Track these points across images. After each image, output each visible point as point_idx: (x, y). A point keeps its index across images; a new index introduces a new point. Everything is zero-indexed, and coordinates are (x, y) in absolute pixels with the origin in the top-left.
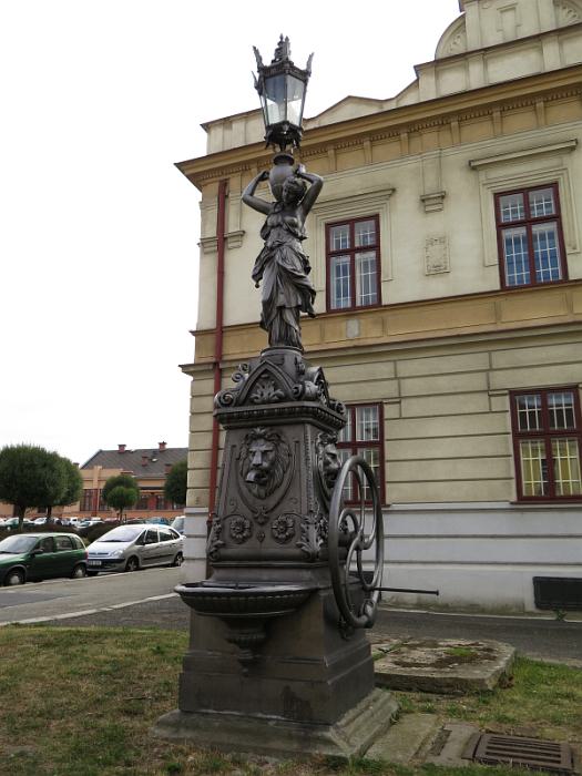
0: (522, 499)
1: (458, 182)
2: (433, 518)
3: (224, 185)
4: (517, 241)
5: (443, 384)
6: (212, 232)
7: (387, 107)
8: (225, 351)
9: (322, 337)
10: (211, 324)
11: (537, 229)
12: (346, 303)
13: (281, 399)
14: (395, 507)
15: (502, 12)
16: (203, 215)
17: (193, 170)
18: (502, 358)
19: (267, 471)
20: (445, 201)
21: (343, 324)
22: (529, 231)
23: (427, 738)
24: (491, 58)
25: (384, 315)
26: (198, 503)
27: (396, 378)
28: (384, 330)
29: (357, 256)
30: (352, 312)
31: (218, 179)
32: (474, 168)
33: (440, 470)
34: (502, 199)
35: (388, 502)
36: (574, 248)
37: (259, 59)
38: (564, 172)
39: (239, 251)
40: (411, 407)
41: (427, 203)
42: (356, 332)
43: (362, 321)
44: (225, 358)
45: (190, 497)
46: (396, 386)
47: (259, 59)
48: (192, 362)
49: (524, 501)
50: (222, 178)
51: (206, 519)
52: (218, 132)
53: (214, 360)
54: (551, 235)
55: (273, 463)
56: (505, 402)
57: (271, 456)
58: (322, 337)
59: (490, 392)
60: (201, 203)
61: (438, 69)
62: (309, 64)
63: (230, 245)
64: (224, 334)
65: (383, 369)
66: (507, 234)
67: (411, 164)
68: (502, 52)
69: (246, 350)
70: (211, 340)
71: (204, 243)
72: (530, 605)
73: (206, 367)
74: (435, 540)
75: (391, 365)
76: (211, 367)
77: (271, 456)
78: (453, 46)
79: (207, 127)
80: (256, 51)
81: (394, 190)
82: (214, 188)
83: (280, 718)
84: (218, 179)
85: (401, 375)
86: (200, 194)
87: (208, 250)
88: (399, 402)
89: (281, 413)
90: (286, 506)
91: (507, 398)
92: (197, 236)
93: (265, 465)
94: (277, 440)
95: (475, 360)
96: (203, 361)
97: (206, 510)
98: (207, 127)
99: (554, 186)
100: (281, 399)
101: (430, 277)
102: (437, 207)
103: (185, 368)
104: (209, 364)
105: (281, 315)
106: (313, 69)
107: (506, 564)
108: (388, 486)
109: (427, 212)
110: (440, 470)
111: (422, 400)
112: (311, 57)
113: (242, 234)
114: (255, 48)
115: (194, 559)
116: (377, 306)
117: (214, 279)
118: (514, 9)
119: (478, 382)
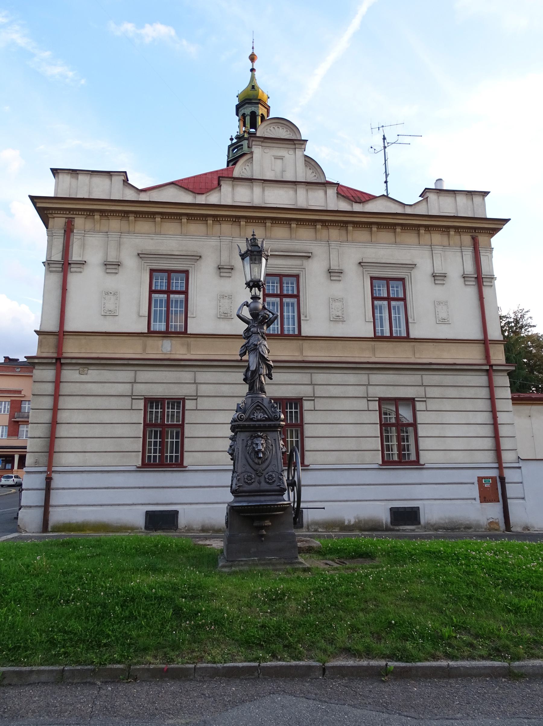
0: (384, 462)
2: (214, 475)
4: (161, 301)
7: (409, 211)
8: (64, 350)
9: (144, 349)
11: (285, 300)
12: (160, 326)
14: (190, 468)
15: (275, 158)
17: (45, 208)
18: (145, 375)
20: (233, 271)
21: (160, 342)
22: (168, 297)
24: (267, 186)
25: (189, 340)
26: (36, 463)
27: (195, 383)
28: (189, 350)
29: (172, 296)
30: (167, 334)
34: (155, 274)
35: (185, 464)
36: (306, 317)
38: (304, 270)
39: (79, 275)
41: (222, 270)
42: (169, 349)
43: (174, 342)
44: (65, 355)
46: (195, 388)
49: (387, 463)
51: (44, 476)
52: (66, 179)
54: (293, 305)
56: (375, 405)
58: (144, 349)
59: (133, 397)
61: (235, 183)
63: (72, 270)
65: (186, 375)
66: (155, 296)
67: (213, 242)
68: (273, 185)
69: (83, 351)
70: (52, 340)
71: (48, 264)
73: (50, 361)
74: (215, 489)
75: (132, 374)
76: (54, 361)
78: (244, 170)
79: (55, 172)
81: (200, 257)
85: (310, 386)
87: (51, 269)
88: (197, 399)
90: (270, 468)
91: (377, 403)
95: (126, 375)
96: (44, 355)
98: (55, 172)
99: (297, 276)
102: (114, 271)
104: (52, 358)
107: (89, 505)
108: (186, 454)
109: (221, 276)
111: (211, 399)
113: (83, 263)
115: (30, 507)
116: (184, 333)
117: (58, 293)
118: (282, 159)
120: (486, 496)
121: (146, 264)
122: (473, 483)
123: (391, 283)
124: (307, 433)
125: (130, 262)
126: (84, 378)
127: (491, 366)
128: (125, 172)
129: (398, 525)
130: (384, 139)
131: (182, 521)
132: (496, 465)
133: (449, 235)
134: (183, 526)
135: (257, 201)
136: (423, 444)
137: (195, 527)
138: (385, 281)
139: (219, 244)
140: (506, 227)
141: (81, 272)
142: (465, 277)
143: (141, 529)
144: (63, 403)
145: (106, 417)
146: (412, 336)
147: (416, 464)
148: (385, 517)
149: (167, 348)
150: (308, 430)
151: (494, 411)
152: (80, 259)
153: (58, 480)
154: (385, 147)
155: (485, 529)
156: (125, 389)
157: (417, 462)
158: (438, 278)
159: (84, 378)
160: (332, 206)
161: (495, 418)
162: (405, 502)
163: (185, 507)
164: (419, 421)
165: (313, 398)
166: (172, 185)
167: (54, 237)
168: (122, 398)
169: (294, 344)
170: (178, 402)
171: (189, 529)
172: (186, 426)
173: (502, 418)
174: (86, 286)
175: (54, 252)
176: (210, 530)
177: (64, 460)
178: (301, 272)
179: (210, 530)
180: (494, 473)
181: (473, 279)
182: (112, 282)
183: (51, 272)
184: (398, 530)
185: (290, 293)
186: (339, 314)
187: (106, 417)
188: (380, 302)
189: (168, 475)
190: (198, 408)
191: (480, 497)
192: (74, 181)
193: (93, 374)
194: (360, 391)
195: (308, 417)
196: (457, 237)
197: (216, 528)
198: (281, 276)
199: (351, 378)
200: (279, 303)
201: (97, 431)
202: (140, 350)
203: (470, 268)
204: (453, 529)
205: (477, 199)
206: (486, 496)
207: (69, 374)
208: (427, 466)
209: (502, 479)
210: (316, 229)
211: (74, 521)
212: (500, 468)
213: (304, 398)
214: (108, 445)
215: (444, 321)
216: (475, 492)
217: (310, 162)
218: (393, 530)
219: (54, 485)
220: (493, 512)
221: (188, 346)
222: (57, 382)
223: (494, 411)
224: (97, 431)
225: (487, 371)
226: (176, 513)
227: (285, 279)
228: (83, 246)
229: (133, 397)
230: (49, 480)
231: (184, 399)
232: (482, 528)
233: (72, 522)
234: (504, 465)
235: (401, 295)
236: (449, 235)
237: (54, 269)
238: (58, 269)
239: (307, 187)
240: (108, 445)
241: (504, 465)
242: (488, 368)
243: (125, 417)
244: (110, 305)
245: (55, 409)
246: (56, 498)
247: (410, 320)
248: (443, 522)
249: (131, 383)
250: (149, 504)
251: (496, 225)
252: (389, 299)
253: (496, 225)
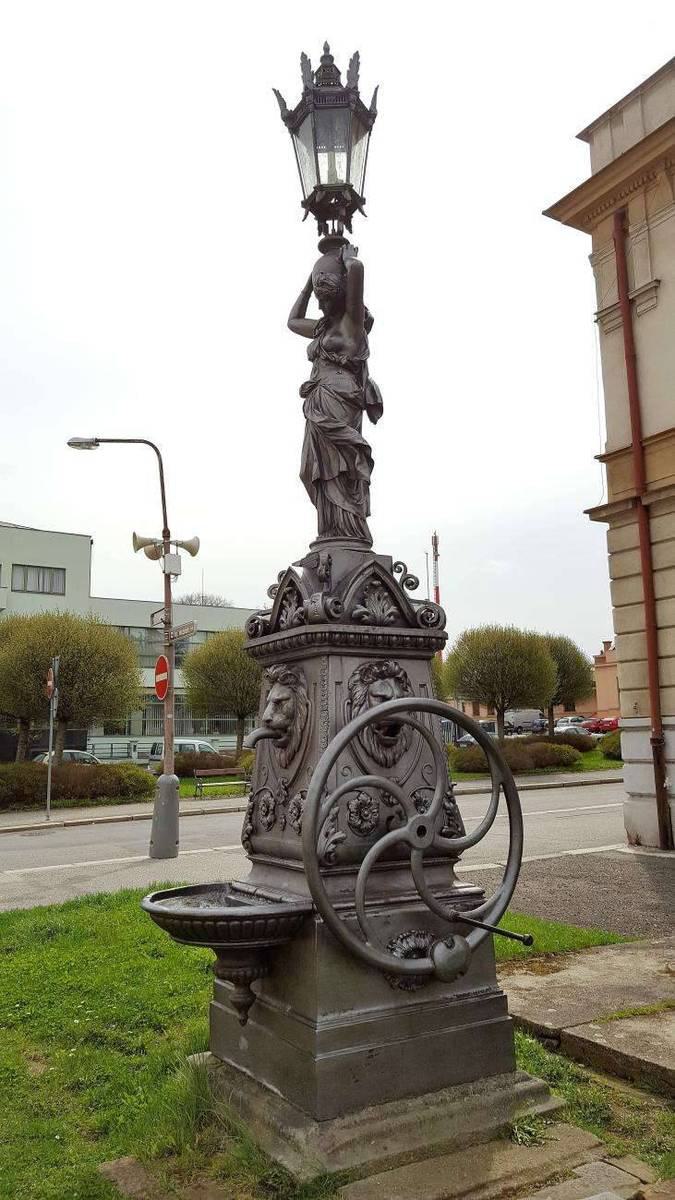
3: (622, 218)
6: (613, 297)
10: (626, 439)
16: (598, 275)
17: (569, 211)
19: (284, 729)
23: (348, 1127)
31: (611, 211)
37: (282, 103)
47: (282, 103)
48: (605, 501)
51: (649, 735)
52: (604, 135)
53: (634, 494)
55: (291, 716)
57: (288, 705)
60: (591, 257)
63: (639, 310)
64: (648, 451)
70: (628, 464)
71: (602, 317)
77: (288, 705)
79: (586, 135)
80: (277, 93)
82: (608, 227)
83: (279, 1093)
84: (611, 211)
86: (589, 237)
92: (592, 306)
93: (278, 719)
94: (290, 682)
96: (622, 497)
97: (648, 722)
98: (586, 135)
103: (595, 514)
104: (626, 501)
105: (322, 492)
106: (378, 107)
112: (377, 89)
114: (274, 90)
117: (623, 371)
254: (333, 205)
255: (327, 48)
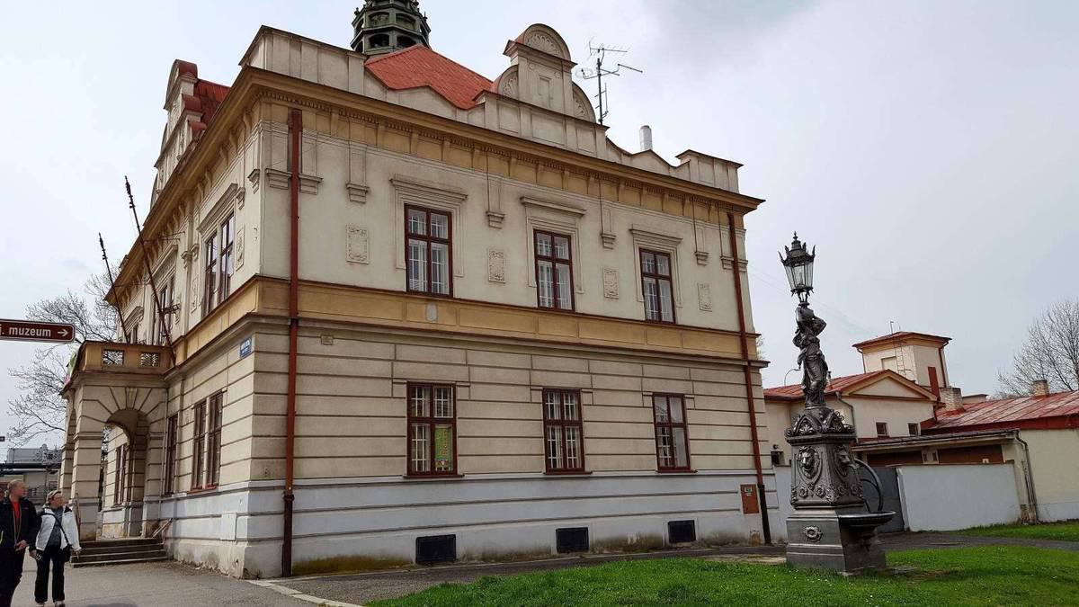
0: (661, 469)
1: (512, 210)
2: (492, 486)
5: (501, 375)
7: (626, 161)
9: (405, 315)
12: (420, 284)
13: (814, 433)
18: (407, 351)
27: (589, 373)
28: (458, 322)
29: (433, 244)
32: (524, 204)
33: (499, 446)
36: (580, 289)
40: (478, 391)
43: (440, 308)
45: (226, 477)
50: (295, 106)
58: (405, 315)
59: (393, 380)
62: (813, 252)
65: (456, 355)
67: (479, 178)
70: (281, 292)
71: (746, 263)
72: (554, 552)
75: (391, 349)
78: (507, 87)
89: (813, 440)
95: (382, 349)
99: (569, 237)
100: (814, 433)
101: (607, 299)
103: (766, 364)
110: (499, 446)
113: (317, 182)
117: (283, 221)
118: (548, 81)
119: (522, 377)
120: (748, 508)
121: (401, 196)
122: (737, 493)
123: (433, 215)
124: (587, 433)
125: (381, 190)
126: (328, 350)
127: (749, 362)
128: (266, 32)
129: (676, 543)
130: (599, 64)
131: (461, 548)
132: (755, 472)
133: (442, 145)
134: (461, 555)
135: (525, 133)
136: (695, 447)
137: (475, 555)
138: (425, 213)
139: (485, 182)
140: (760, 206)
141: (315, 194)
142: (723, 259)
143: (412, 562)
144: (304, 385)
145: (361, 407)
146: (456, 295)
147: (687, 471)
148: (664, 533)
149: (431, 315)
150: (589, 429)
151: (751, 412)
152: (313, 174)
153: (301, 500)
154: (600, 75)
155: (749, 543)
156: (383, 368)
157: (687, 469)
158: (701, 257)
159: (328, 350)
160: (356, 88)
161: (753, 419)
162: (678, 515)
163: (463, 529)
164: (689, 420)
165: (591, 390)
166: (426, 90)
167: (273, 134)
168: (381, 381)
169: (570, 322)
170: (446, 389)
171: (468, 557)
172: (458, 422)
173: (759, 419)
174: (325, 212)
175: (275, 156)
176: (491, 559)
177: (307, 469)
178: (454, 210)
179: (491, 559)
180: (753, 481)
181: (730, 263)
182: (357, 215)
183: (272, 186)
184: (676, 548)
185: (545, 254)
186: (613, 289)
187: (361, 407)
188: (416, 242)
189: (442, 487)
190: (472, 398)
191: (744, 507)
192: (295, 53)
193: (340, 346)
194: (633, 384)
195: (587, 413)
196: (484, 159)
197: (498, 555)
198: (553, 235)
199: (626, 367)
200: (426, 248)
201: (349, 427)
202: (398, 316)
203: (727, 251)
204: (723, 544)
205: (731, 171)
206: (748, 508)
207: (308, 344)
208: (699, 473)
209: (761, 487)
210: (377, 129)
211: (325, 557)
212: (759, 475)
213: (458, 384)
214: (363, 447)
215: (706, 308)
216: (737, 501)
217: (577, 92)
218: (671, 548)
219: (296, 505)
220: (753, 524)
221: (457, 315)
222: (293, 354)
223: (751, 412)
224: (349, 427)
225: (745, 367)
226: (454, 537)
227: (433, 215)
228: (316, 156)
229: (393, 380)
230: (288, 500)
231: (454, 386)
232: (746, 542)
233: (321, 559)
234: (763, 472)
235: (445, 236)
236: (442, 145)
237: (277, 184)
238: (282, 184)
239: (578, 125)
240: (363, 447)
241: (763, 472)
242: (746, 364)
243: (384, 407)
244: (358, 248)
245: (291, 395)
246: (301, 525)
247: (677, 304)
248: (713, 536)
249: (389, 360)
250: (429, 527)
251: (752, 203)
252: (429, 239)
253: (752, 203)
254: (802, 289)
255: (796, 238)
